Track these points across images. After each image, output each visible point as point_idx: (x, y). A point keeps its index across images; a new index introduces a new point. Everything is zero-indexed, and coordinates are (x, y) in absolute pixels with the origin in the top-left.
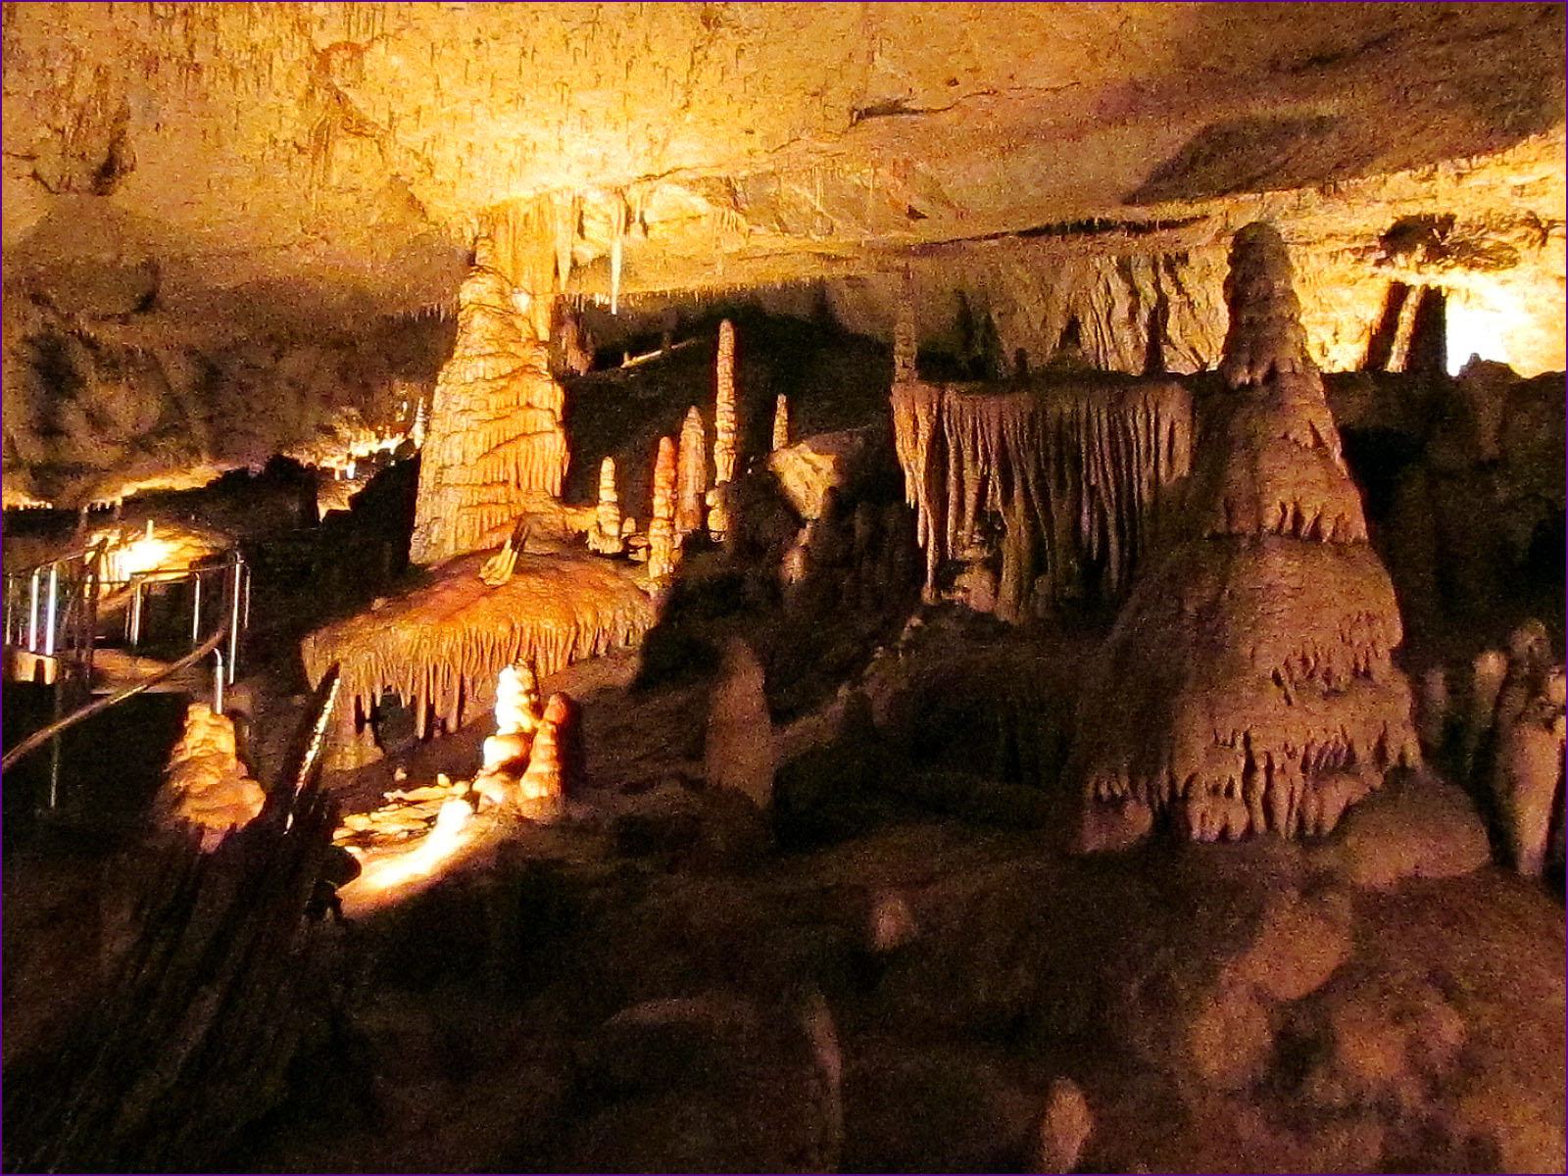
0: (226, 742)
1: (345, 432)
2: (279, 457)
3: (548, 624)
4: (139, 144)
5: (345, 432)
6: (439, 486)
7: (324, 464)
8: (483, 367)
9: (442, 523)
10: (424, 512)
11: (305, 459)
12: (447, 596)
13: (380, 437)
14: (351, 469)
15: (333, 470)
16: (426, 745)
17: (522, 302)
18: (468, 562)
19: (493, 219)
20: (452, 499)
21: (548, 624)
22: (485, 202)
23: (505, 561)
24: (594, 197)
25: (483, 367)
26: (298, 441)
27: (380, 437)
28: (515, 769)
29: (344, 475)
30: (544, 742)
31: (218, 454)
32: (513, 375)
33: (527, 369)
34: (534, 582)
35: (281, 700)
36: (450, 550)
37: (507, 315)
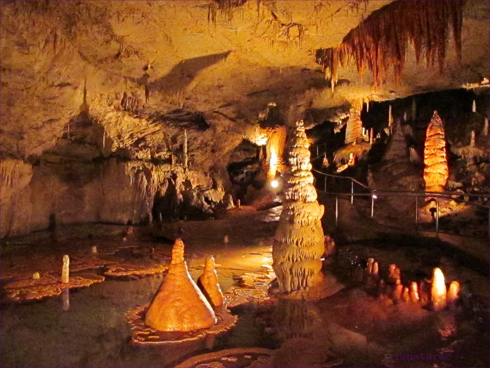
0: (327, 161)
1: (339, 114)
2: (326, 121)
3: (360, 150)
4: (314, 101)
5: (339, 114)
6: (348, 134)
7: (335, 121)
8: (352, 120)
9: (349, 138)
10: (346, 137)
11: (331, 121)
12: (348, 147)
13: (346, 114)
14: (341, 122)
15: (337, 123)
16: (343, 162)
17: (357, 111)
18: (351, 143)
19: (353, 100)
20: (349, 136)
21: (360, 150)
22: (352, 99)
23: (355, 143)
24: (365, 98)
25: (352, 120)
26: (329, 117)
27: (346, 114)
28: (351, 162)
29: (339, 123)
30: (354, 160)
31: (315, 121)
32: (356, 120)
33: (358, 120)
34: (358, 145)
35: (330, 158)
36: (349, 142)
37: (355, 113)
